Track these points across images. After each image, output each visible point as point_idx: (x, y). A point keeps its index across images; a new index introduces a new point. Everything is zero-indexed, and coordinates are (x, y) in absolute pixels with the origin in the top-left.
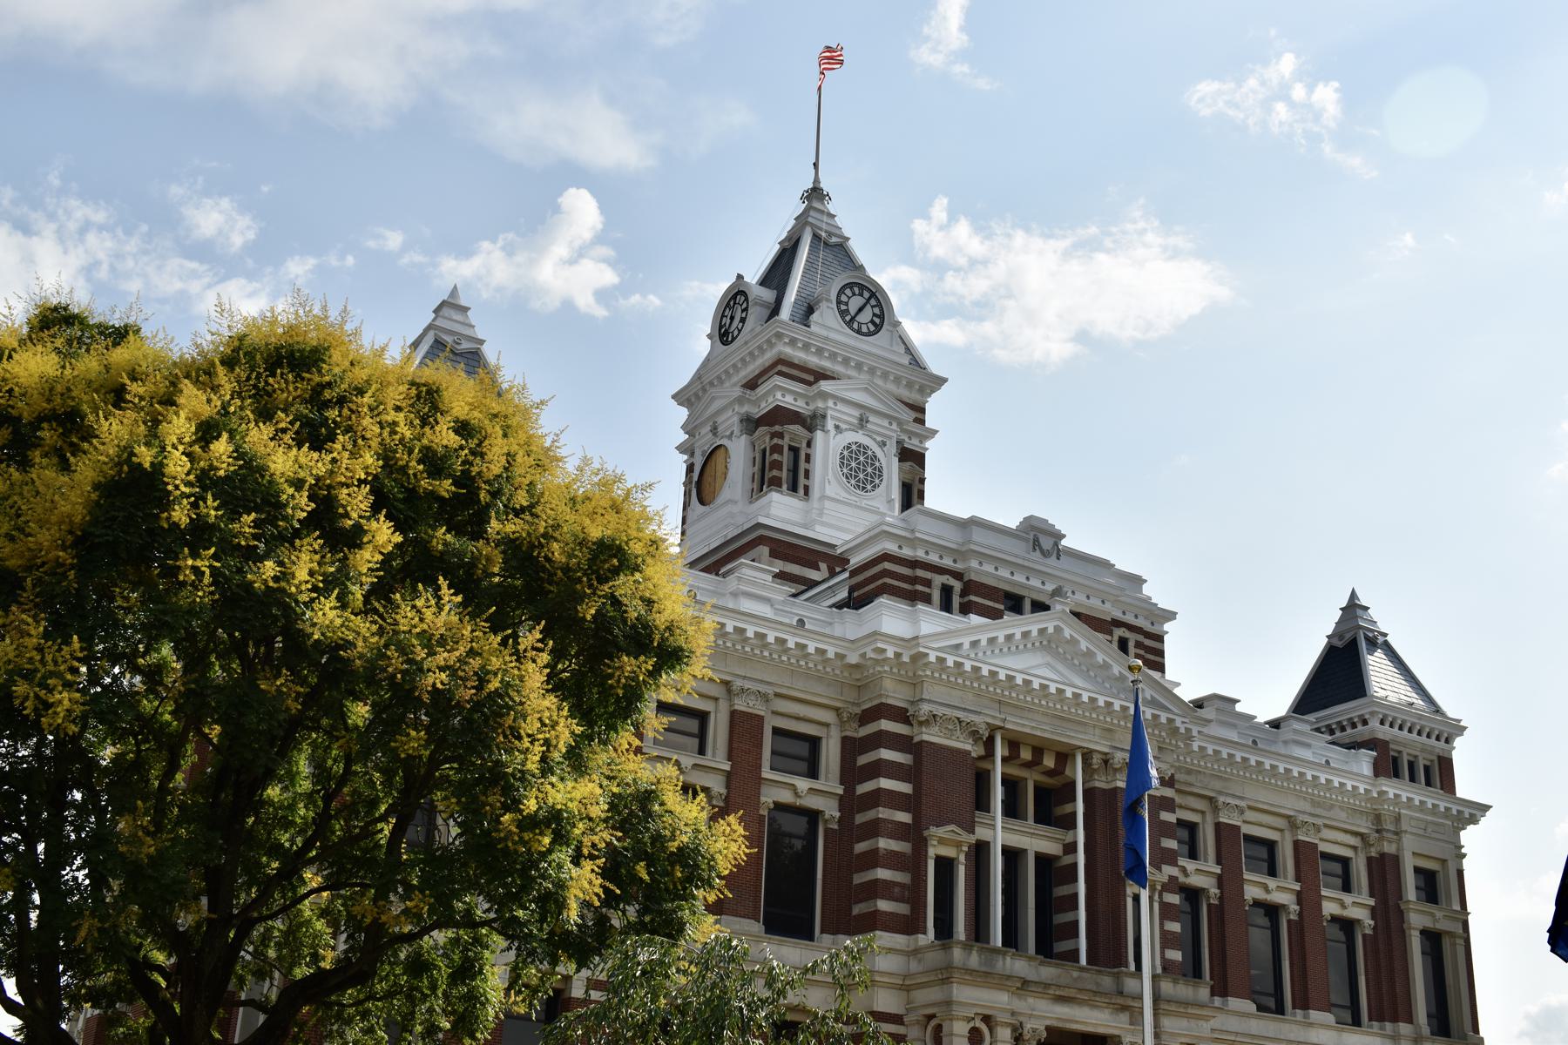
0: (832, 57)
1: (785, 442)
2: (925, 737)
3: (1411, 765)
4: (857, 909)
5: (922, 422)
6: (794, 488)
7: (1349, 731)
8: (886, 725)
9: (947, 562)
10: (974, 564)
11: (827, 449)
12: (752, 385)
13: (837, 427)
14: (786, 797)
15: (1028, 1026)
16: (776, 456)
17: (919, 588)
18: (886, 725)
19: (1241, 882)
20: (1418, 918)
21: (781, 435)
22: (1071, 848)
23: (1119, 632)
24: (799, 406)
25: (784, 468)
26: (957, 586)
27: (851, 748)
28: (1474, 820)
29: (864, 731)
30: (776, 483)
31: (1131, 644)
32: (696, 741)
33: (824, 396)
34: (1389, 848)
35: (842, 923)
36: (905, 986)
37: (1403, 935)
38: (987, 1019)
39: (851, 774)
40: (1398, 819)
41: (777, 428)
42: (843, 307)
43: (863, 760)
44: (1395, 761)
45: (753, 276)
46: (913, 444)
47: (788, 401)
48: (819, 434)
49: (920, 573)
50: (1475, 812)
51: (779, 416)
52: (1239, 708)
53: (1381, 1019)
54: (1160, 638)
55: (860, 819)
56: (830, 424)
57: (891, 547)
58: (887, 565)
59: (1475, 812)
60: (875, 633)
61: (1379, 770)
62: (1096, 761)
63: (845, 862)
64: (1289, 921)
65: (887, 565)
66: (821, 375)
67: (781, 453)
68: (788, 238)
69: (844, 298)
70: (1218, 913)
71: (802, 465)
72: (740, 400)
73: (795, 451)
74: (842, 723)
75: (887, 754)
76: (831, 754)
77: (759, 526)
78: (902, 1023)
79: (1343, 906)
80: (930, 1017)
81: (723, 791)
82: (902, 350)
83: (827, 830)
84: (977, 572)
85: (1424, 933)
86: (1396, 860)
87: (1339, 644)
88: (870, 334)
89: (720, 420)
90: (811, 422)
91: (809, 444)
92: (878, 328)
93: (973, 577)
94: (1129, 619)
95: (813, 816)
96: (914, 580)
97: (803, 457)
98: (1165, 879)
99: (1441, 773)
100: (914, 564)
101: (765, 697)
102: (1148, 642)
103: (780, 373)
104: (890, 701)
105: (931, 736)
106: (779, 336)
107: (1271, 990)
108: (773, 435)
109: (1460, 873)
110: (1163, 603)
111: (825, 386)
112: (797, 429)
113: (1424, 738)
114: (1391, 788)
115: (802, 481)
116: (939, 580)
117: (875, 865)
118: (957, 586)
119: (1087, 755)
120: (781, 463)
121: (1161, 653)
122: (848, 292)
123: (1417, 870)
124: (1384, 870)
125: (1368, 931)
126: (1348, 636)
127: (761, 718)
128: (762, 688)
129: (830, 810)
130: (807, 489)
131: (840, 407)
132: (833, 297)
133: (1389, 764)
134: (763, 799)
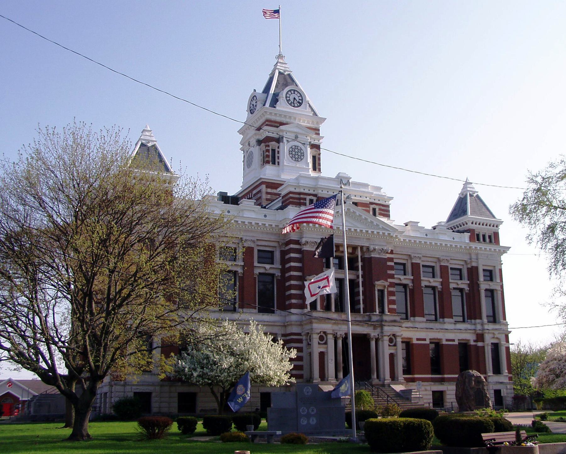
0: (277, 12)
1: (270, 148)
2: (305, 249)
3: (484, 236)
4: (287, 303)
5: (319, 134)
6: (274, 163)
7: (462, 226)
8: (292, 246)
9: (311, 192)
10: (320, 191)
11: (285, 148)
12: (259, 129)
13: (287, 141)
14: (262, 271)
15: (339, 333)
16: (267, 153)
17: (302, 201)
18: (292, 246)
19: (420, 280)
20: (484, 285)
21: (269, 146)
22: (358, 277)
23: (372, 206)
24: (275, 136)
25: (271, 158)
26: (315, 199)
27: (283, 253)
28: (505, 252)
29: (287, 248)
30: (268, 162)
31: (377, 210)
32: (431, 274)
33: (282, 131)
34: (474, 264)
35: (284, 307)
36: (301, 324)
37: (479, 292)
38: (325, 333)
39: (284, 261)
40: (477, 254)
41: (267, 144)
42: (288, 99)
43: (287, 257)
44: (478, 235)
45: (260, 90)
46: (316, 142)
47: (270, 135)
48: (281, 144)
49: (302, 196)
50: (506, 249)
51: (268, 140)
52: (419, 225)
53: (471, 319)
54: (388, 206)
55: (287, 275)
56: (285, 139)
57: (292, 190)
58: (291, 195)
59: (506, 249)
60: (286, 219)
61: (471, 239)
62: (365, 249)
63: (283, 288)
64: (439, 291)
65: (291, 195)
66: (282, 124)
67: (269, 152)
68: (271, 74)
69: (288, 96)
70: (412, 291)
71: (277, 155)
72: (255, 134)
73: (273, 151)
74: (280, 246)
75: (293, 255)
76: (277, 256)
77: (261, 179)
78: (301, 335)
79: (458, 284)
80: (308, 333)
81: (242, 272)
82: (310, 110)
83: (277, 280)
84: (321, 194)
85: (486, 290)
86: (477, 268)
87: (462, 196)
88: (298, 107)
89: (250, 141)
90: (279, 140)
91: (278, 148)
92: (300, 104)
93: (320, 195)
94: (373, 201)
95: (273, 275)
96: (300, 199)
97: (276, 152)
98: (388, 283)
99: (494, 238)
100: (300, 194)
101: (254, 242)
102: (383, 208)
103: (267, 125)
104: (293, 239)
105: (306, 248)
106: (266, 112)
107: (434, 313)
108: (266, 146)
109: (501, 270)
110: (389, 195)
111: (282, 127)
112: (274, 143)
113: (488, 227)
114: (475, 245)
115: (277, 160)
116: (308, 198)
117: (290, 289)
118: (315, 199)
119: (362, 247)
120: (269, 155)
121: (389, 211)
122: (290, 93)
123: (484, 270)
124: (473, 272)
125: (467, 292)
126: (465, 193)
127: (253, 248)
128: (253, 239)
129: (278, 274)
130: (278, 163)
131: (288, 134)
132: (284, 96)
133: (475, 237)
134: (255, 272)
